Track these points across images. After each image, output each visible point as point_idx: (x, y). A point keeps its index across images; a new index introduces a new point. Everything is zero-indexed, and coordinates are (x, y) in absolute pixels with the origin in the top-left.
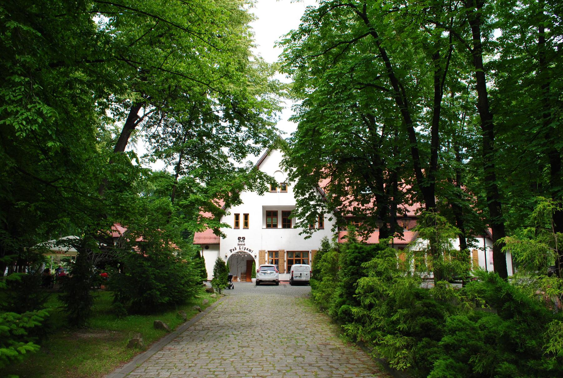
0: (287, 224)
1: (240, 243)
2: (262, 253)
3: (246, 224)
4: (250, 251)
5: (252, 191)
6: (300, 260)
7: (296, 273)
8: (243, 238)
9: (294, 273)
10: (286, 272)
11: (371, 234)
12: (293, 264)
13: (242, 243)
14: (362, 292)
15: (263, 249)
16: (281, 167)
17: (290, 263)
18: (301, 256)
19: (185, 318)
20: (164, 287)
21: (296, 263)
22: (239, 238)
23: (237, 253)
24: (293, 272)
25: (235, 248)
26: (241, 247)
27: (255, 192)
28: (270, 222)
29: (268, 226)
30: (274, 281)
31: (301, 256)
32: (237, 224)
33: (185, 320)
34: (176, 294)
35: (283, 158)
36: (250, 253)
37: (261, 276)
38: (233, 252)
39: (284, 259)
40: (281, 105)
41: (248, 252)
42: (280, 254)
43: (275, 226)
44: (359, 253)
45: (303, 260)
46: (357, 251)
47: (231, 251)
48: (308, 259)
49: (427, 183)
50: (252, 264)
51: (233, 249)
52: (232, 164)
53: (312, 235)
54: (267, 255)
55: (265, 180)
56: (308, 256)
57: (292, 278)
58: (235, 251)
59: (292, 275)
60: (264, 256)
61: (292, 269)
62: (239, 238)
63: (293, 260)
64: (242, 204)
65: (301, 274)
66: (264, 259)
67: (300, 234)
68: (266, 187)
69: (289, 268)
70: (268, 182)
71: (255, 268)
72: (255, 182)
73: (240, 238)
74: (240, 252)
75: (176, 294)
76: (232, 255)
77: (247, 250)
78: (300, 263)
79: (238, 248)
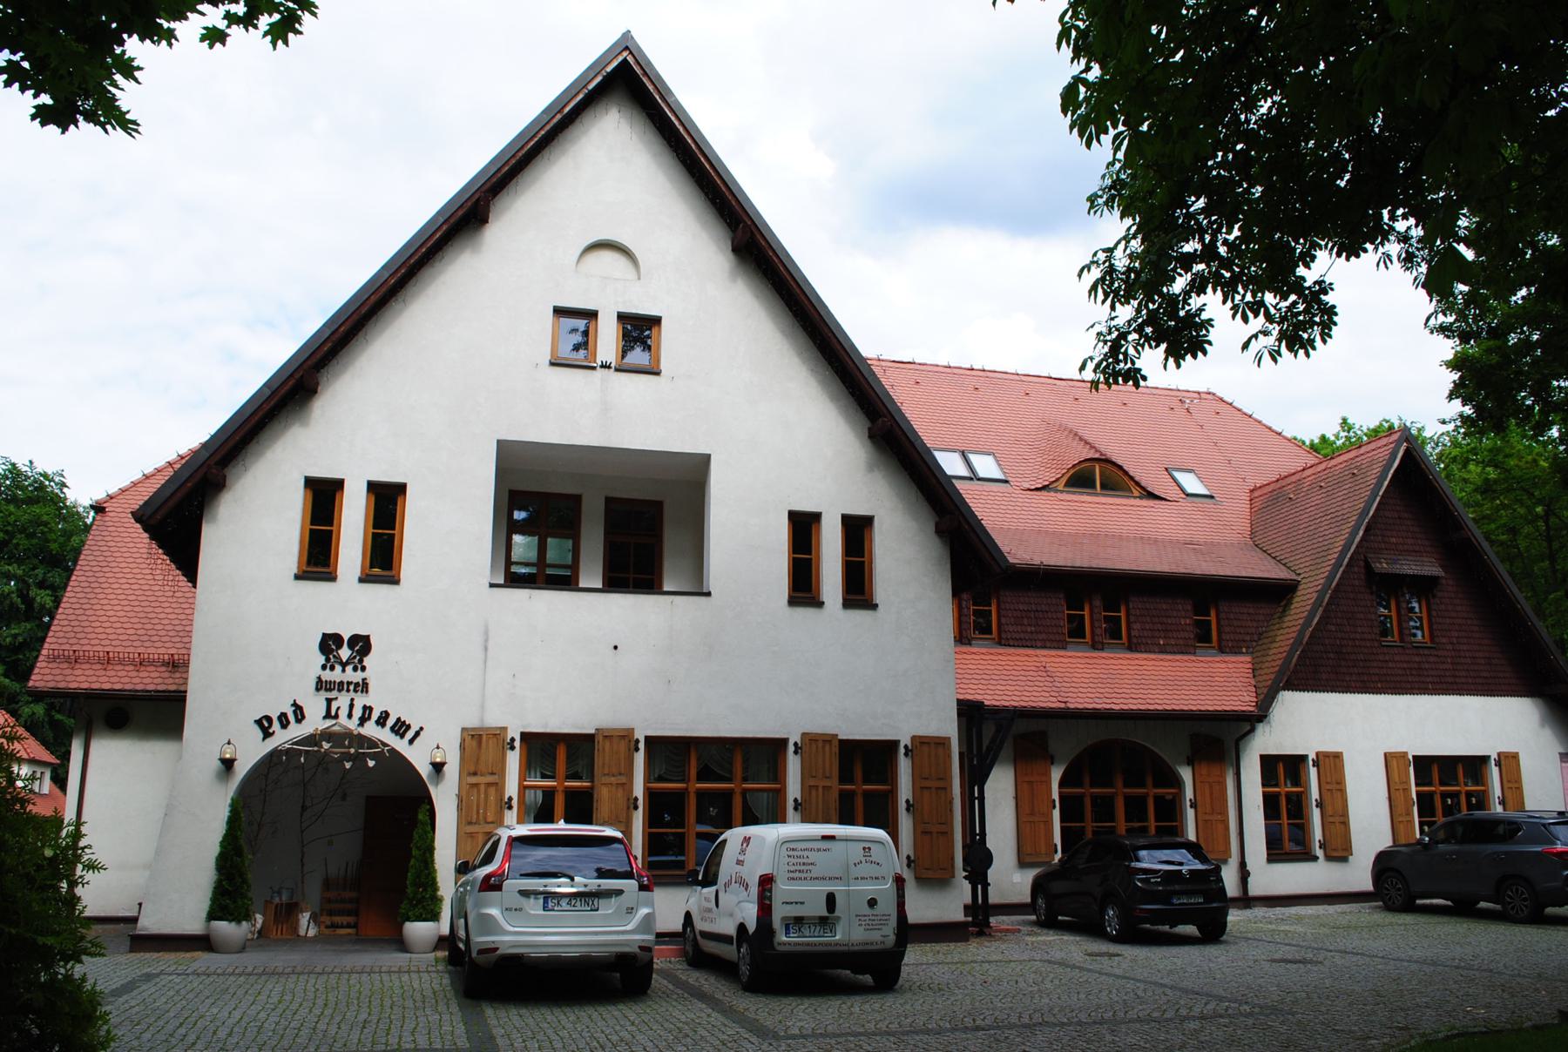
1: (336, 675)
4: (400, 728)
9: (782, 889)
13: (351, 675)
15: (493, 720)
22: (330, 643)
23: (312, 740)
26: (342, 701)
36: (400, 745)
38: (282, 738)
39: (628, 786)
41: (385, 735)
42: (603, 757)
47: (264, 725)
50: (422, 816)
54: (513, 760)
56: (889, 775)
58: (296, 731)
60: (500, 771)
62: (330, 643)
65: (831, 899)
66: (499, 786)
74: (327, 735)
76: (272, 760)
77: (382, 721)
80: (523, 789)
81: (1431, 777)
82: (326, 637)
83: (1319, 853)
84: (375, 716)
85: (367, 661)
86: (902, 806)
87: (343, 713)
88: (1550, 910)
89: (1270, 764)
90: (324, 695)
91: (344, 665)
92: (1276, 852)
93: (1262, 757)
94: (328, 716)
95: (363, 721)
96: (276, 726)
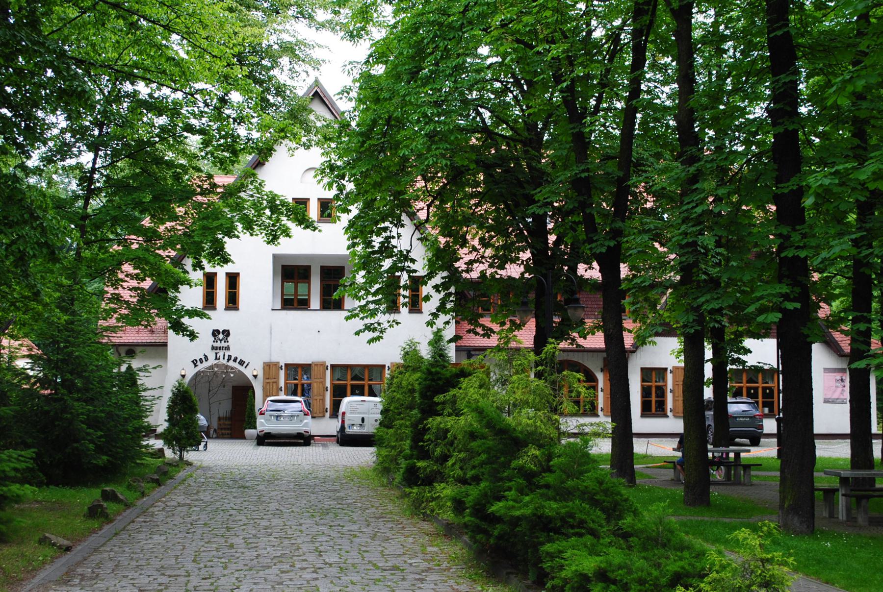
0: (331, 303)
1: (218, 344)
2: (270, 368)
3: (233, 302)
4: (242, 363)
5: (252, 235)
6: (363, 386)
7: (352, 418)
8: (224, 331)
9: (347, 416)
10: (328, 414)
11: (516, 333)
12: (345, 395)
13: (223, 344)
14: (433, 438)
15: (274, 359)
16: (319, 177)
17: (339, 393)
18: (366, 377)
19: (142, 490)
20: (101, 437)
21: (353, 394)
22: (215, 333)
23: (211, 367)
24: (344, 413)
25: (206, 357)
26: (221, 354)
27: (260, 236)
28: (293, 292)
29: (288, 304)
30: (299, 436)
31: (366, 377)
32: (210, 300)
33: (143, 494)
34: (702, 299)
35: (324, 159)
36: (242, 368)
37: (264, 424)
38: (201, 367)
39: (323, 382)
40: (317, 54)
41: (236, 365)
42: (314, 371)
43: (303, 304)
44: (433, 380)
45: (370, 386)
46: (430, 377)
47: (195, 363)
48: (666, 385)
49: (602, 245)
50: (250, 394)
51: (201, 360)
52: (210, 176)
53: (385, 335)
54: (282, 374)
55: (282, 213)
56: (664, 379)
57: (343, 428)
58: (206, 364)
59: (343, 422)
60: (277, 377)
61: (343, 408)
62: (215, 333)
63: (345, 386)
64: (230, 264)
65: (363, 420)
66: (277, 383)
67: (357, 333)
68: (284, 225)
69: (336, 405)
70: (288, 216)
71: (253, 406)
72: (259, 215)
73: (218, 331)
74: (217, 365)
75: (702, 299)
76: (197, 375)
77: (235, 360)
78: (363, 395)
79: (211, 356)
80: (286, 384)
81: (742, 379)
82: (228, 331)
83: (669, 413)
84: (233, 358)
85: (229, 339)
86: (669, 391)
87: (221, 358)
88: (737, 440)
89: (647, 373)
90: (215, 351)
91: (221, 341)
92: (646, 411)
93: (642, 369)
94: (216, 359)
95: (228, 360)
96: (199, 363)
